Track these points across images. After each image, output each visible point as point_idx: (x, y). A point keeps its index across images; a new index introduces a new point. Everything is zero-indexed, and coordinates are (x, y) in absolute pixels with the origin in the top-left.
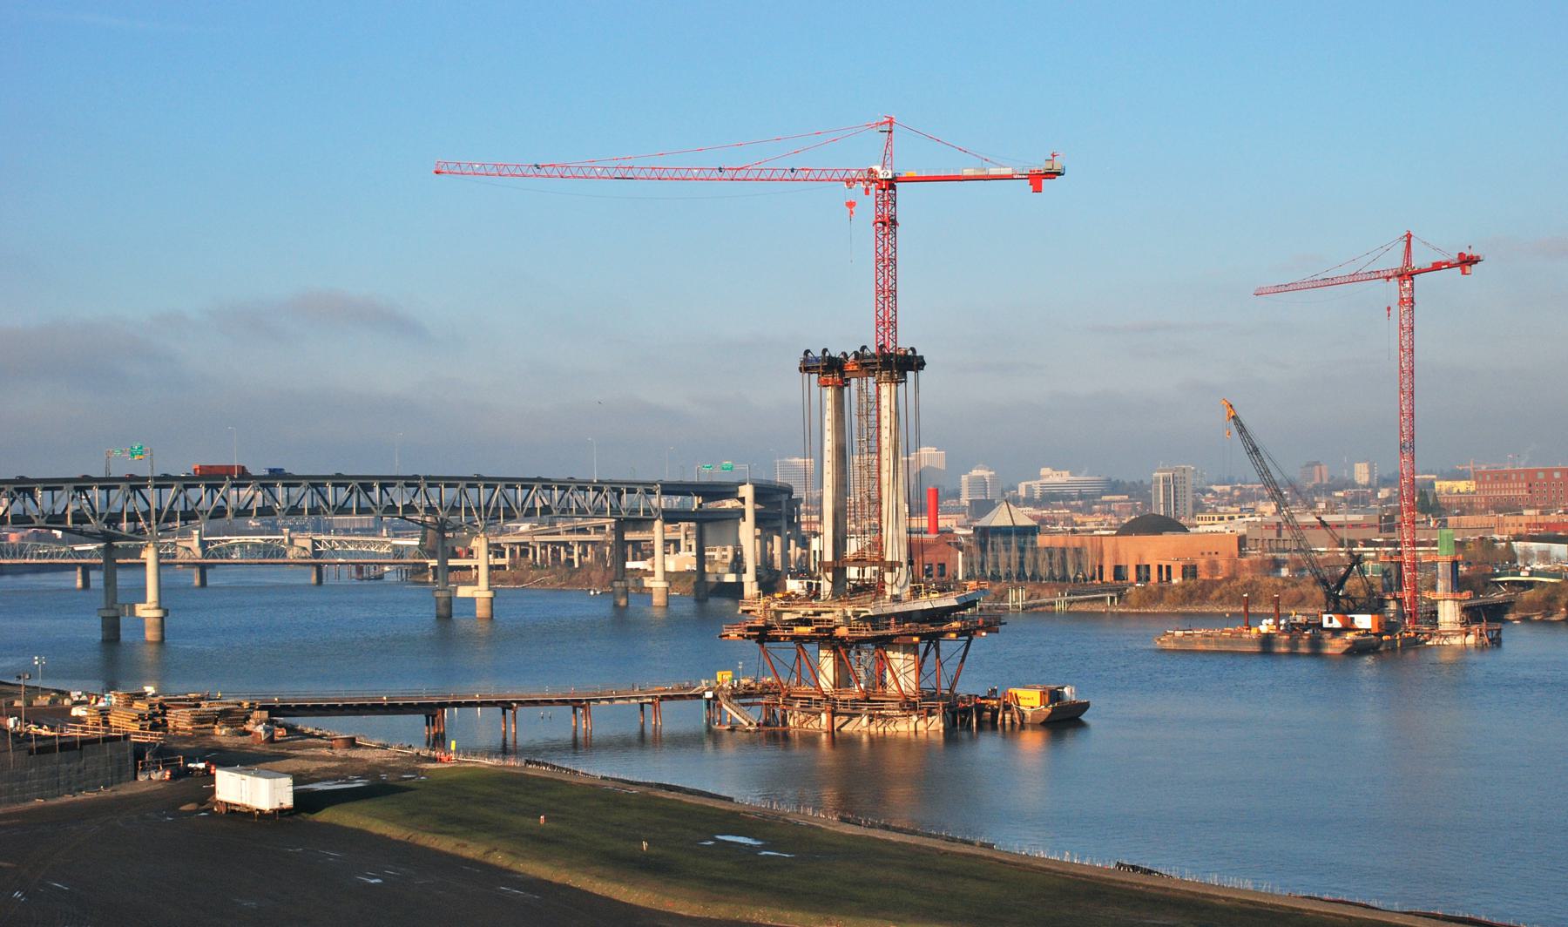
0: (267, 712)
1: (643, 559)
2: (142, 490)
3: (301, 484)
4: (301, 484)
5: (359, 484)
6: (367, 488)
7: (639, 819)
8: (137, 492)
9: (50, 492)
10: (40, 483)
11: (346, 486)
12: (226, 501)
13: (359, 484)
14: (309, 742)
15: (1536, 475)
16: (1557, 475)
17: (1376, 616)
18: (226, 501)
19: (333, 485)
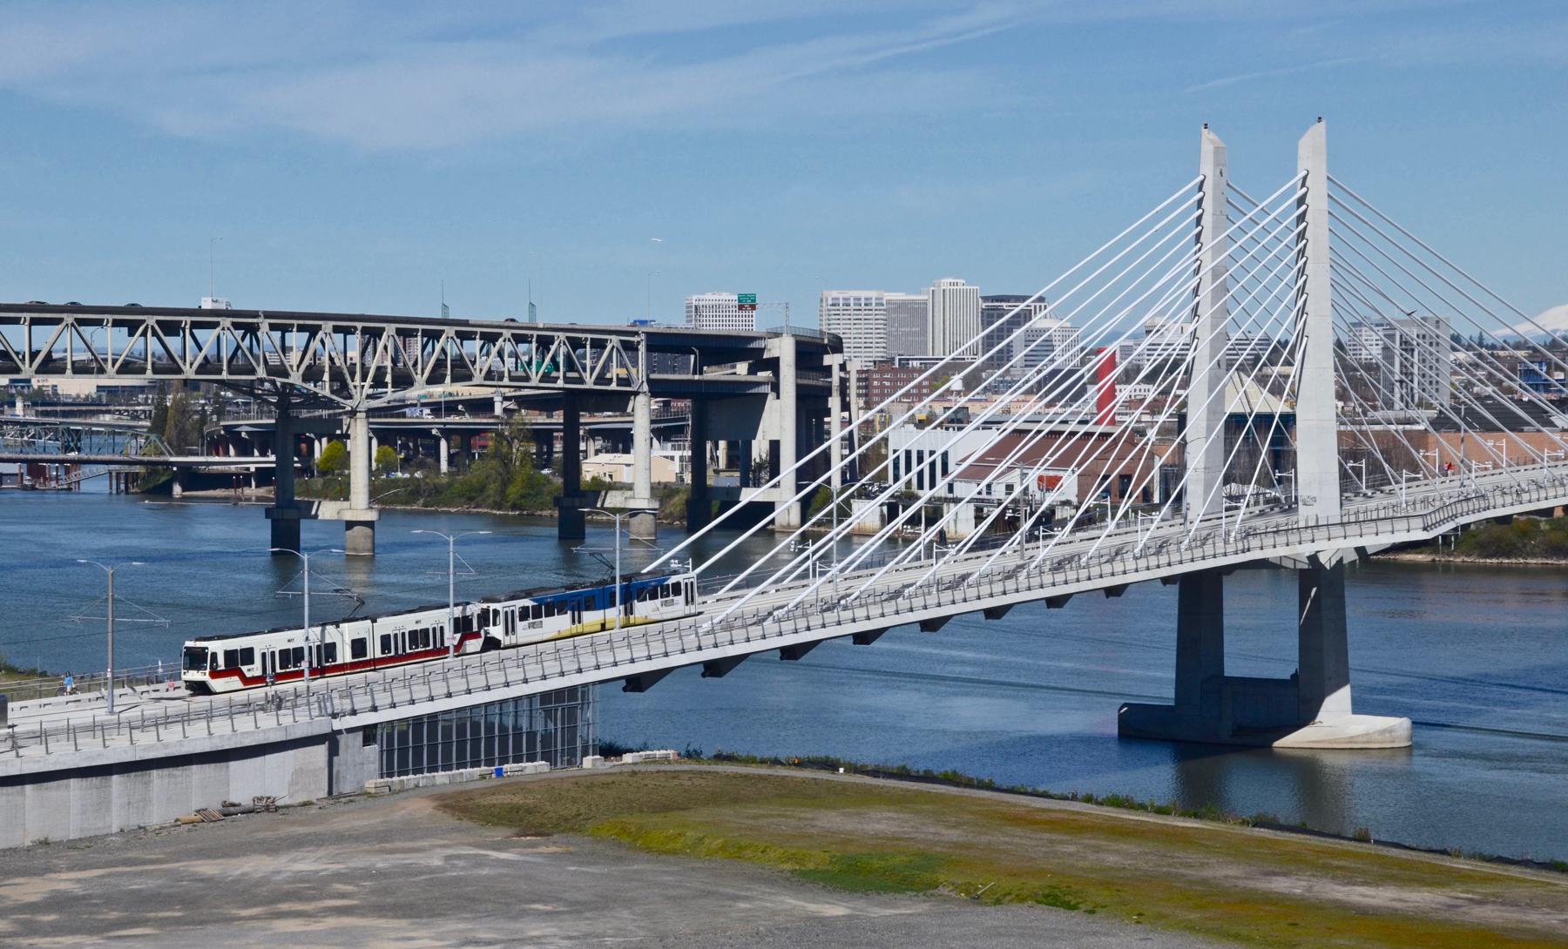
5: (158, 322)
13: (158, 322)
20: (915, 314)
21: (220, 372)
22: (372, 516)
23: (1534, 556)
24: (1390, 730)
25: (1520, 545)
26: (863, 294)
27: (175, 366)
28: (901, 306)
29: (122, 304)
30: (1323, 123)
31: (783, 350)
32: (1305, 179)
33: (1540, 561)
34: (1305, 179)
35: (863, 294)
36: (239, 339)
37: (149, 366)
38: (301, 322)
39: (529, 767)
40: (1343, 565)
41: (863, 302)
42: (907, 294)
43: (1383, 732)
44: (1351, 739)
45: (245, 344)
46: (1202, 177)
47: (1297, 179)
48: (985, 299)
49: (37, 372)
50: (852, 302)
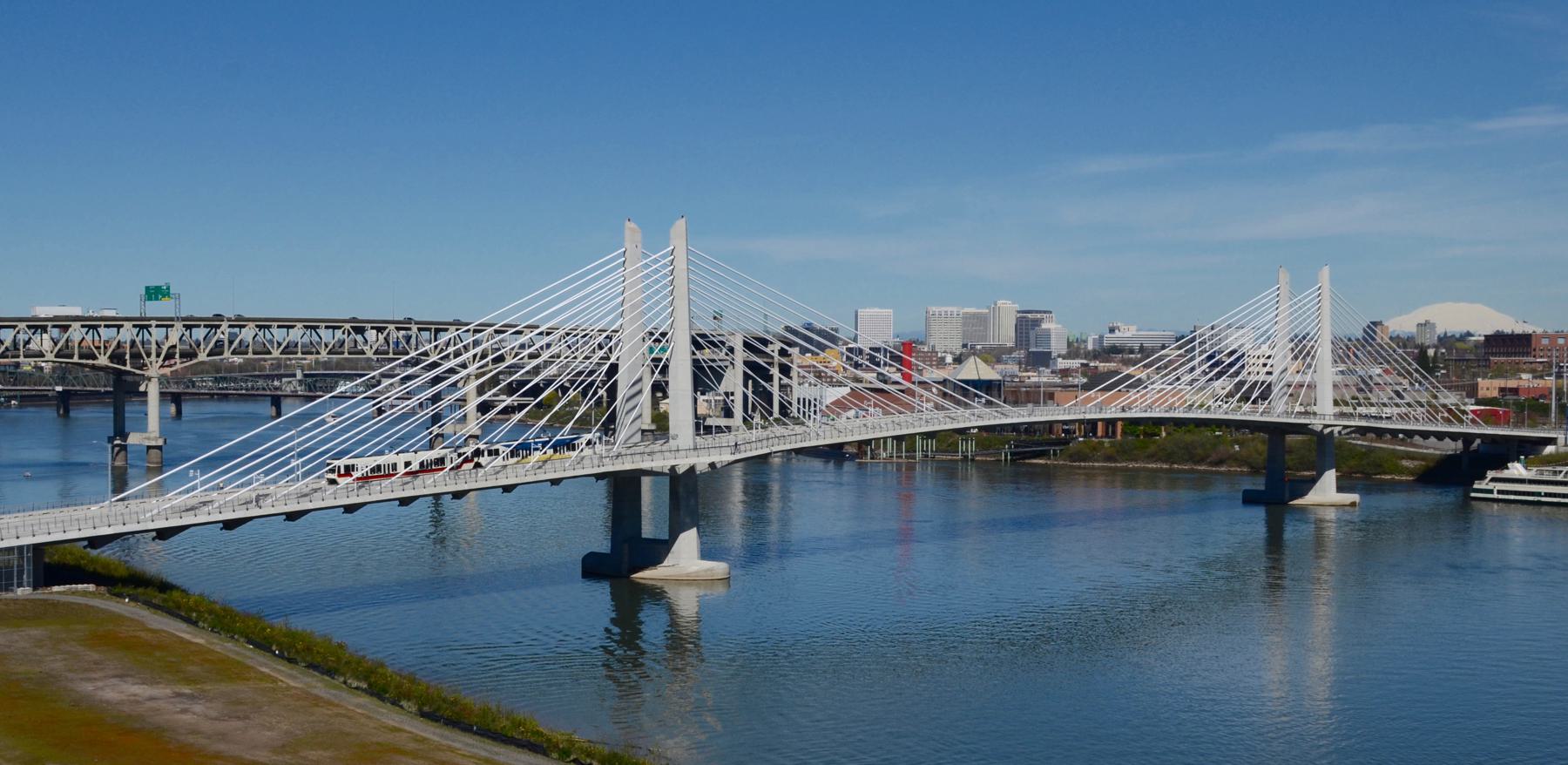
0: (644, 536)
1: (162, 375)
2: (149, 329)
3: (295, 326)
4: (295, 326)
5: (351, 327)
6: (360, 331)
7: (1362, 521)
8: (145, 330)
9: (165, 329)
10: (24, 321)
11: (429, 330)
12: (644, 338)
13: (351, 327)
14: (1304, 476)
15: (1556, 341)
16: (1561, 341)
17: (70, 408)
18: (644, 338)
19: (397, 328)
20: (981, 320)
21: (71, 356)
22: (653, 427)
23: (1098, 461)
24: (711, 570)
25: (1091, 455)
26: (949, 309)
27: (265, 350)
28: (974, 315)
29: (402, 319)
30: (684, 219)
31: (737, 343)
32: (673, 250)
33: (1100, 464)
34: (673, 250)
35: (949, 309)
36: (135, 334)
37: (391, 351)
38: (437, 326)
39: (20, 591)
40: (697, 476)
41: (949, 313)
42: (978, 308)
43: (706, 571)
44: (688, 575)
45: (89, 338)
46: (624, 249)
47: (669, 249)
48: (1019, 312)
49: (232, 354)
50: (943, 313)
